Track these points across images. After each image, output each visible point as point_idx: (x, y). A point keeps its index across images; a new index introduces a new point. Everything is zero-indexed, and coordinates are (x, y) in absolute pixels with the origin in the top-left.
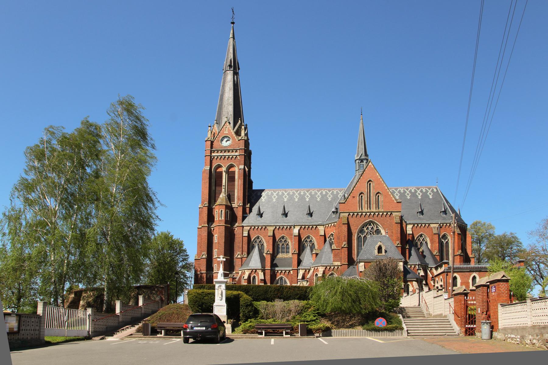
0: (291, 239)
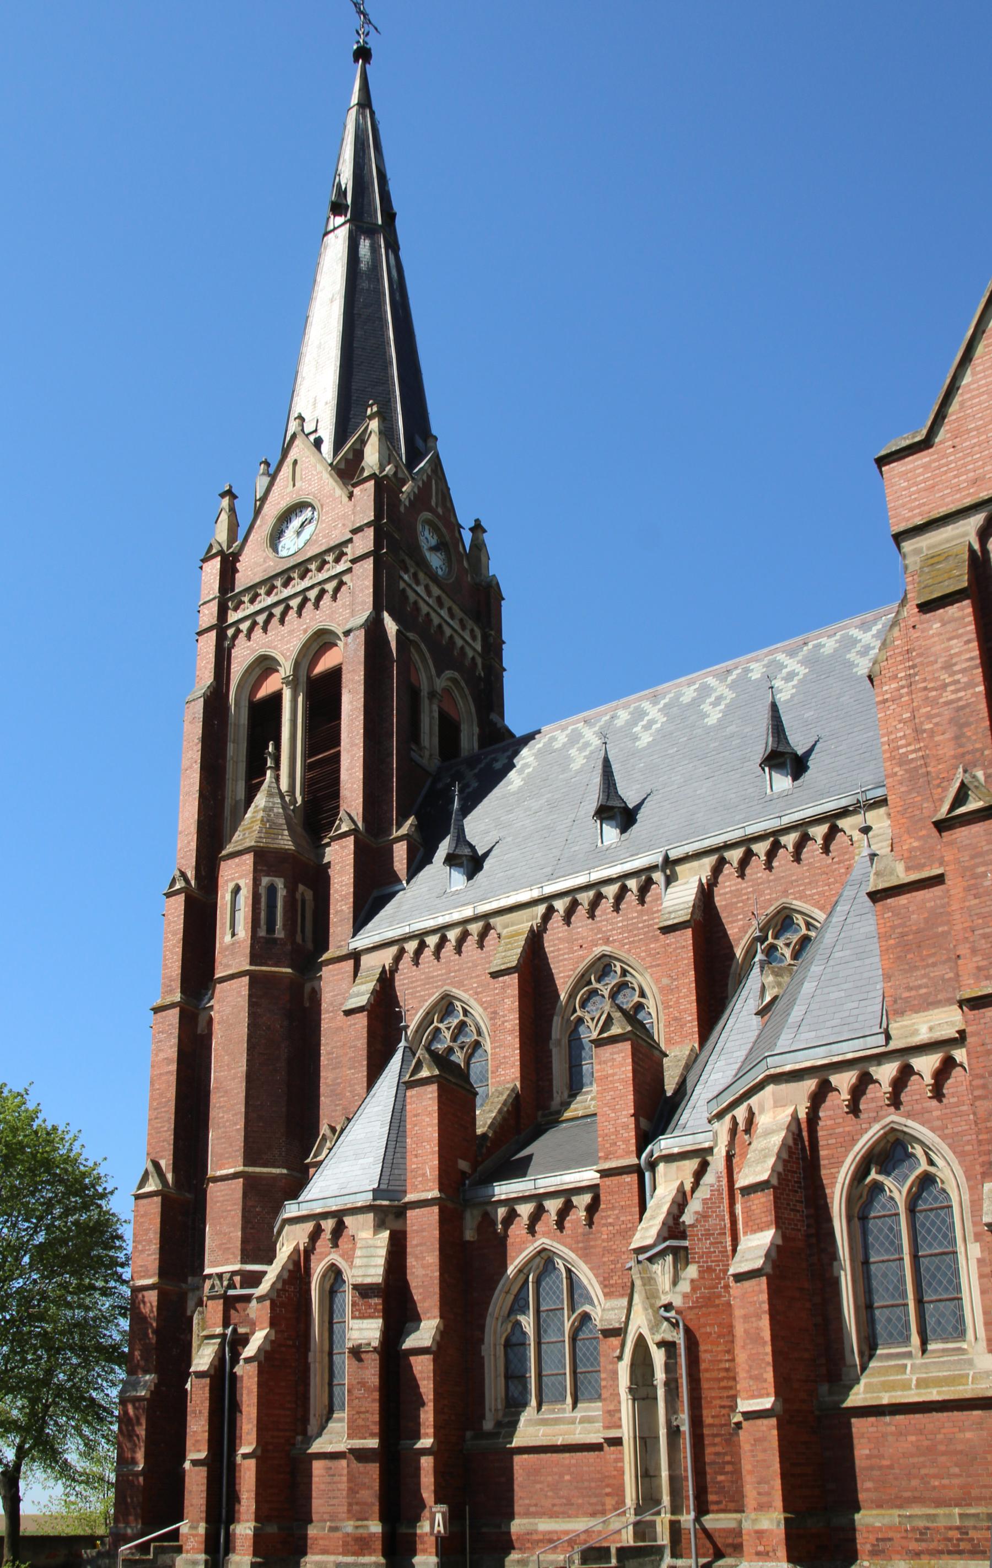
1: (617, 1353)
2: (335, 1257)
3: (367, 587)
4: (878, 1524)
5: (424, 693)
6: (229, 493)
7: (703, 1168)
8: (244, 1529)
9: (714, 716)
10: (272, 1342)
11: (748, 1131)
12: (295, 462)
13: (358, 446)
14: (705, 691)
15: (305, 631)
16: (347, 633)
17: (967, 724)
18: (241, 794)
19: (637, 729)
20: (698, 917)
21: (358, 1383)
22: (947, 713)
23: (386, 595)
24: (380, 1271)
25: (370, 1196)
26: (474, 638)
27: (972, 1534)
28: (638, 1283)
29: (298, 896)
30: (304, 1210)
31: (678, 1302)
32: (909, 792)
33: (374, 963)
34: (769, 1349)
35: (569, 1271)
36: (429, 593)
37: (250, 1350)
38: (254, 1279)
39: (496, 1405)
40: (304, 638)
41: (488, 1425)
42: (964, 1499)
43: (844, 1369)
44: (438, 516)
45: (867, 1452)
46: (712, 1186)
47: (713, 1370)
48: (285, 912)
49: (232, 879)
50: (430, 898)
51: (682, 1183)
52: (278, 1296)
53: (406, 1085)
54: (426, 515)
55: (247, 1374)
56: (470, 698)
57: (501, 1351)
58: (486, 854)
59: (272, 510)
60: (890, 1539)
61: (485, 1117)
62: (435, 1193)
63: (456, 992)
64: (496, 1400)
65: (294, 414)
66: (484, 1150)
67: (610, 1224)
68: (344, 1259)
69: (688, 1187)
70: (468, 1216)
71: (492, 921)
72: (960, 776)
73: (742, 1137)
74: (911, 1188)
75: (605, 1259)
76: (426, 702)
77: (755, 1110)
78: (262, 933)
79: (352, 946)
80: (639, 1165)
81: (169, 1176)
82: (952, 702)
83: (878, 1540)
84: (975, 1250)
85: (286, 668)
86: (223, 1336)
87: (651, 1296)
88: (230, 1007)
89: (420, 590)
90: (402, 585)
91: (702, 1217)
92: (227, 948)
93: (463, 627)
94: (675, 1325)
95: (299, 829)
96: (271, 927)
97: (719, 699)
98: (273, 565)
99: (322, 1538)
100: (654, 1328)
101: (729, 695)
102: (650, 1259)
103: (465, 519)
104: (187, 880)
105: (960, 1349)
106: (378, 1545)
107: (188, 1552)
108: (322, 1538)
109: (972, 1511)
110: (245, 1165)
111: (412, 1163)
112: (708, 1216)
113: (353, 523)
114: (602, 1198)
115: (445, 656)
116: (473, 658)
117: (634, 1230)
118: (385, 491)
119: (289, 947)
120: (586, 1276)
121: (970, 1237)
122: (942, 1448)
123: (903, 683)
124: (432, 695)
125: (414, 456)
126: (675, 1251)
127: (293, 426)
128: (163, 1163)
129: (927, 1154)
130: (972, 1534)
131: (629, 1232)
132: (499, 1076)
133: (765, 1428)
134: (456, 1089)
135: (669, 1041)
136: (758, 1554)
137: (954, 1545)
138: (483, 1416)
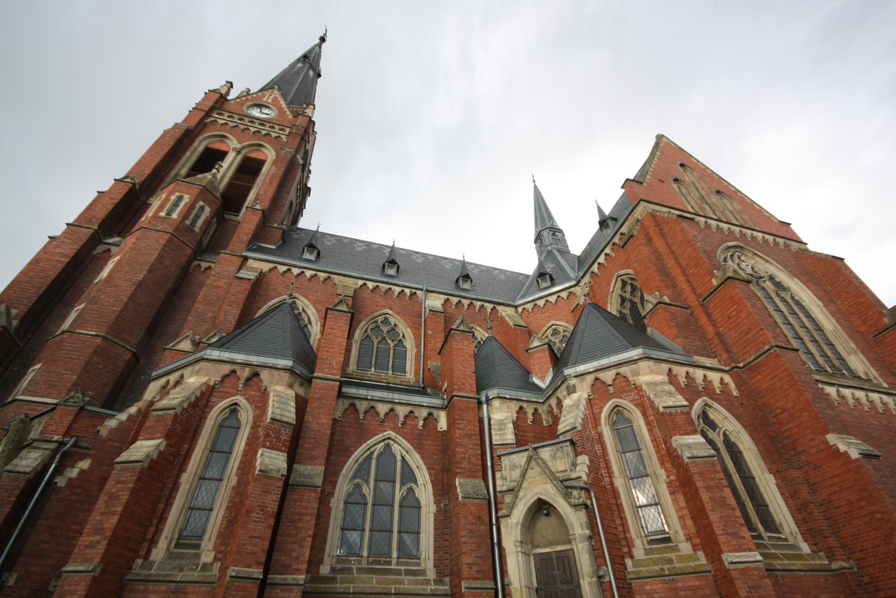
0: (415, 328)
10: (160, 452)
21: (259, 506)
48: (204, 223)
52: (181, 414)
67: (461, 429)
68: (248, 402)
78: (188, 222)
133: (756, 578)
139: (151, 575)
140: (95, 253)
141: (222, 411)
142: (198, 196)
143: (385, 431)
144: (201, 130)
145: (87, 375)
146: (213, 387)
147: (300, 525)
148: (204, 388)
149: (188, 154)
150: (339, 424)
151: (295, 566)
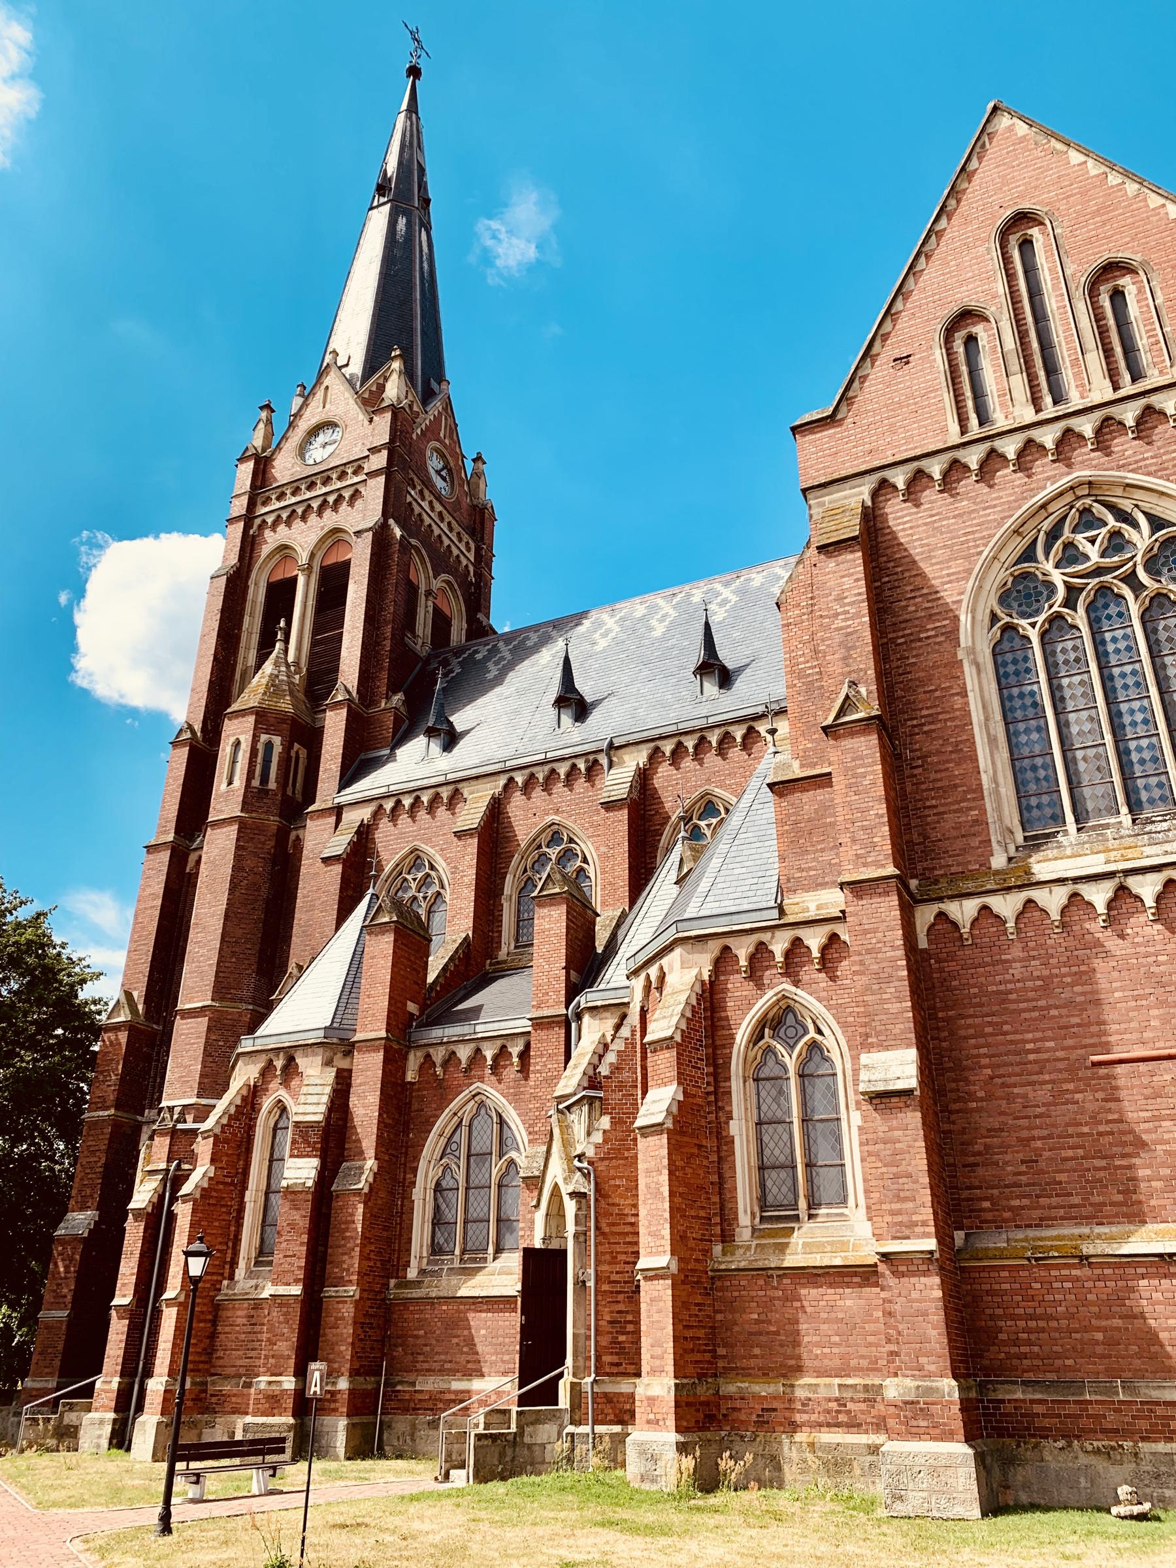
1: (534, 1203)
2: (282, 1093)
3: (378, 498)
4: (763, 1394)
5: (423, 589)
6: (267, 407)
7: (624, 1017)
8: (156, 1385)
9: (659, 630)
11: (660, 989)
12: (327, 388)
13: (381, 381)
14: (653, 609)
15: (322, 528)
16: (358, 533)
17: (854, 647)
18: (252, 660)
19: (597, 636)
20: (635, 795)
22: (838, 638)
23: (393, 505)
24: (323, 1108)
25: (321, 1033)
26: (469, 550)
27: (850, 1406)
28: (556, 1131)
29: (293, 754)
30: (259, 1045)
31: (590, 1153)
32: (806, 701)
33: (354, 818)
34: (667, 1205)
35: (500, 1116)
36: (432, 508)
37: (187, 1188)
38: (202, 1113)
39: (421, 1252)
40: (321, 533)
41: (412, 1274)
42: (844, 1370)
43: (737, 1230)
44: (445, 446)
45: (755, 1316)
46: (627, 1039)
47: (619, 1224)
49: (234, 734)
50: (414, 763)
51: (604, 1035)
52: (223, 1132)
53: (369, 928)
54: (434, 444)
55: (183, 1212)
56: (461, 598)
57: (430, 1195)
58: (467, 732)
59: (304, 425)
60: (775, 1410)
61: (436, 964)
62: (383, 1034)
63: (423, 847)
64: (422, 1246)
65: (330, 349)
66: (433, 994)
69: (609, 1039)
70: (411, 1057)
71: (459, 786)
72: (845, 690)
73: (655, 994)
74: (800, 1054)
75: (531, 1106)
76: (423, 598)
77: (666, 970)
78: (256, 783)
79: (337, 801)
80: (567, 1015)
81: (140, 1007)
82: (841, 628)
83: (763, 1409)
84: (856, 1118)
85: (303, 558)
86: (167, 1170)
87: (567, 1144)
88: (218, 850)
89: (425, 505)
90: (409, 499)
91: (616, 1068)
92: (221, 796)
93: (460, 540)
94: (587, 1176)
95: (301, 696)
96: (265, 779)
97: (665, 616)
98: (300, 471)
99: (235, 1395)
100: (566, 1180)
101: (673, 613)
102: (568, 1108)
103: (469, 451)
104: (193, 732)
105: (842, 1214)
106: (289, 1403)
107: (97, 1410)
108: (235, 1395)
109: (849, 1381)
110: (213, 1000)
111: (364, 1003)
112: (623, 1069)
113: (372, 443)
114: (533, 1045)
115: (442, 562)
116: (467, 566)
117: (558, 1078)
118: (401, 420)
119: (279, 797)
120: (513, 1117)
121: (852, 1106)
122: (824, 1315)
123: (805, 610)
124: (429, 593)
125: (428, 395)
126: (591, 1100)
127: (328, 358)
128: (135, 994)
129: (814, 1022)
130: (850, 1406)
131: (554, 1080)
132: (453, 926)
134: (412, 938)
135: (603, 903)
136: (649, 1422)
137: (833, 1418)
138: (408, 1264)
139: (234, 1294)
140: (188, 870)
141: (270, 1112)
142: (255, 729)
143: (471, 1084)
144: (251, 558)
145: (211, 1059)
146: (255, 1086)
147: (348, 1234)
148: (244, 1092)
149: (246, 619)
150: (416, 1087)
151: (347, 1278)
